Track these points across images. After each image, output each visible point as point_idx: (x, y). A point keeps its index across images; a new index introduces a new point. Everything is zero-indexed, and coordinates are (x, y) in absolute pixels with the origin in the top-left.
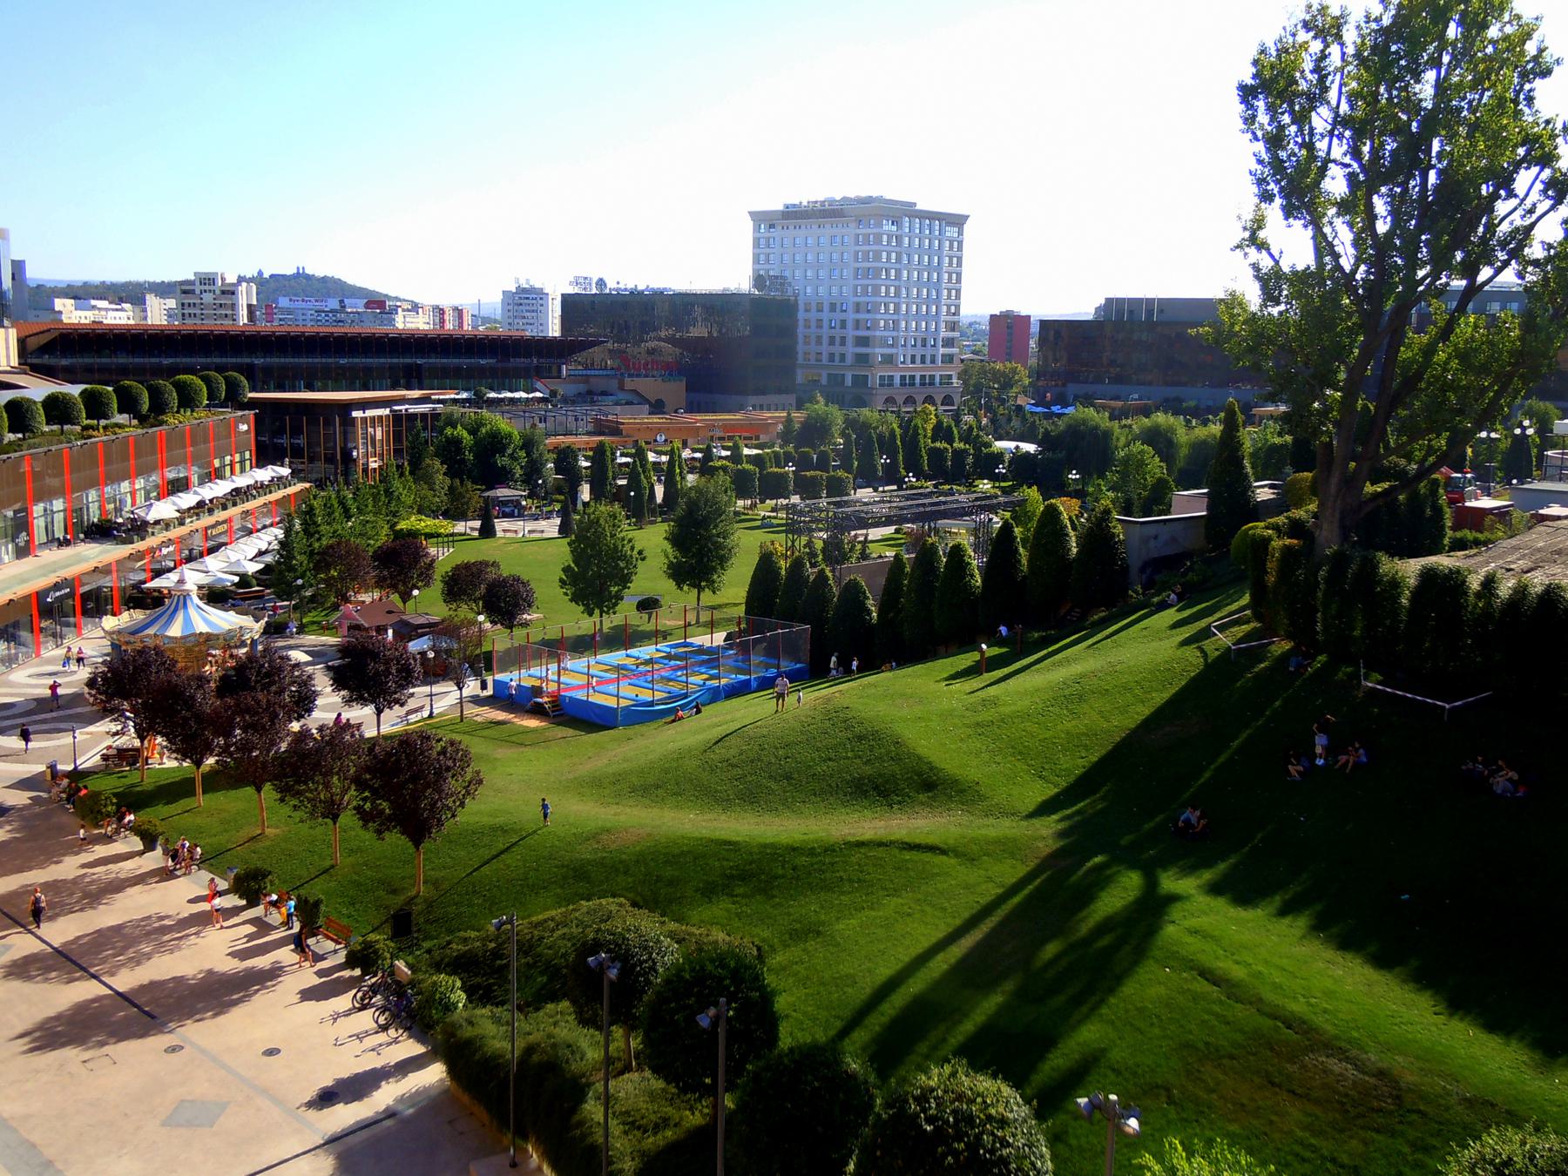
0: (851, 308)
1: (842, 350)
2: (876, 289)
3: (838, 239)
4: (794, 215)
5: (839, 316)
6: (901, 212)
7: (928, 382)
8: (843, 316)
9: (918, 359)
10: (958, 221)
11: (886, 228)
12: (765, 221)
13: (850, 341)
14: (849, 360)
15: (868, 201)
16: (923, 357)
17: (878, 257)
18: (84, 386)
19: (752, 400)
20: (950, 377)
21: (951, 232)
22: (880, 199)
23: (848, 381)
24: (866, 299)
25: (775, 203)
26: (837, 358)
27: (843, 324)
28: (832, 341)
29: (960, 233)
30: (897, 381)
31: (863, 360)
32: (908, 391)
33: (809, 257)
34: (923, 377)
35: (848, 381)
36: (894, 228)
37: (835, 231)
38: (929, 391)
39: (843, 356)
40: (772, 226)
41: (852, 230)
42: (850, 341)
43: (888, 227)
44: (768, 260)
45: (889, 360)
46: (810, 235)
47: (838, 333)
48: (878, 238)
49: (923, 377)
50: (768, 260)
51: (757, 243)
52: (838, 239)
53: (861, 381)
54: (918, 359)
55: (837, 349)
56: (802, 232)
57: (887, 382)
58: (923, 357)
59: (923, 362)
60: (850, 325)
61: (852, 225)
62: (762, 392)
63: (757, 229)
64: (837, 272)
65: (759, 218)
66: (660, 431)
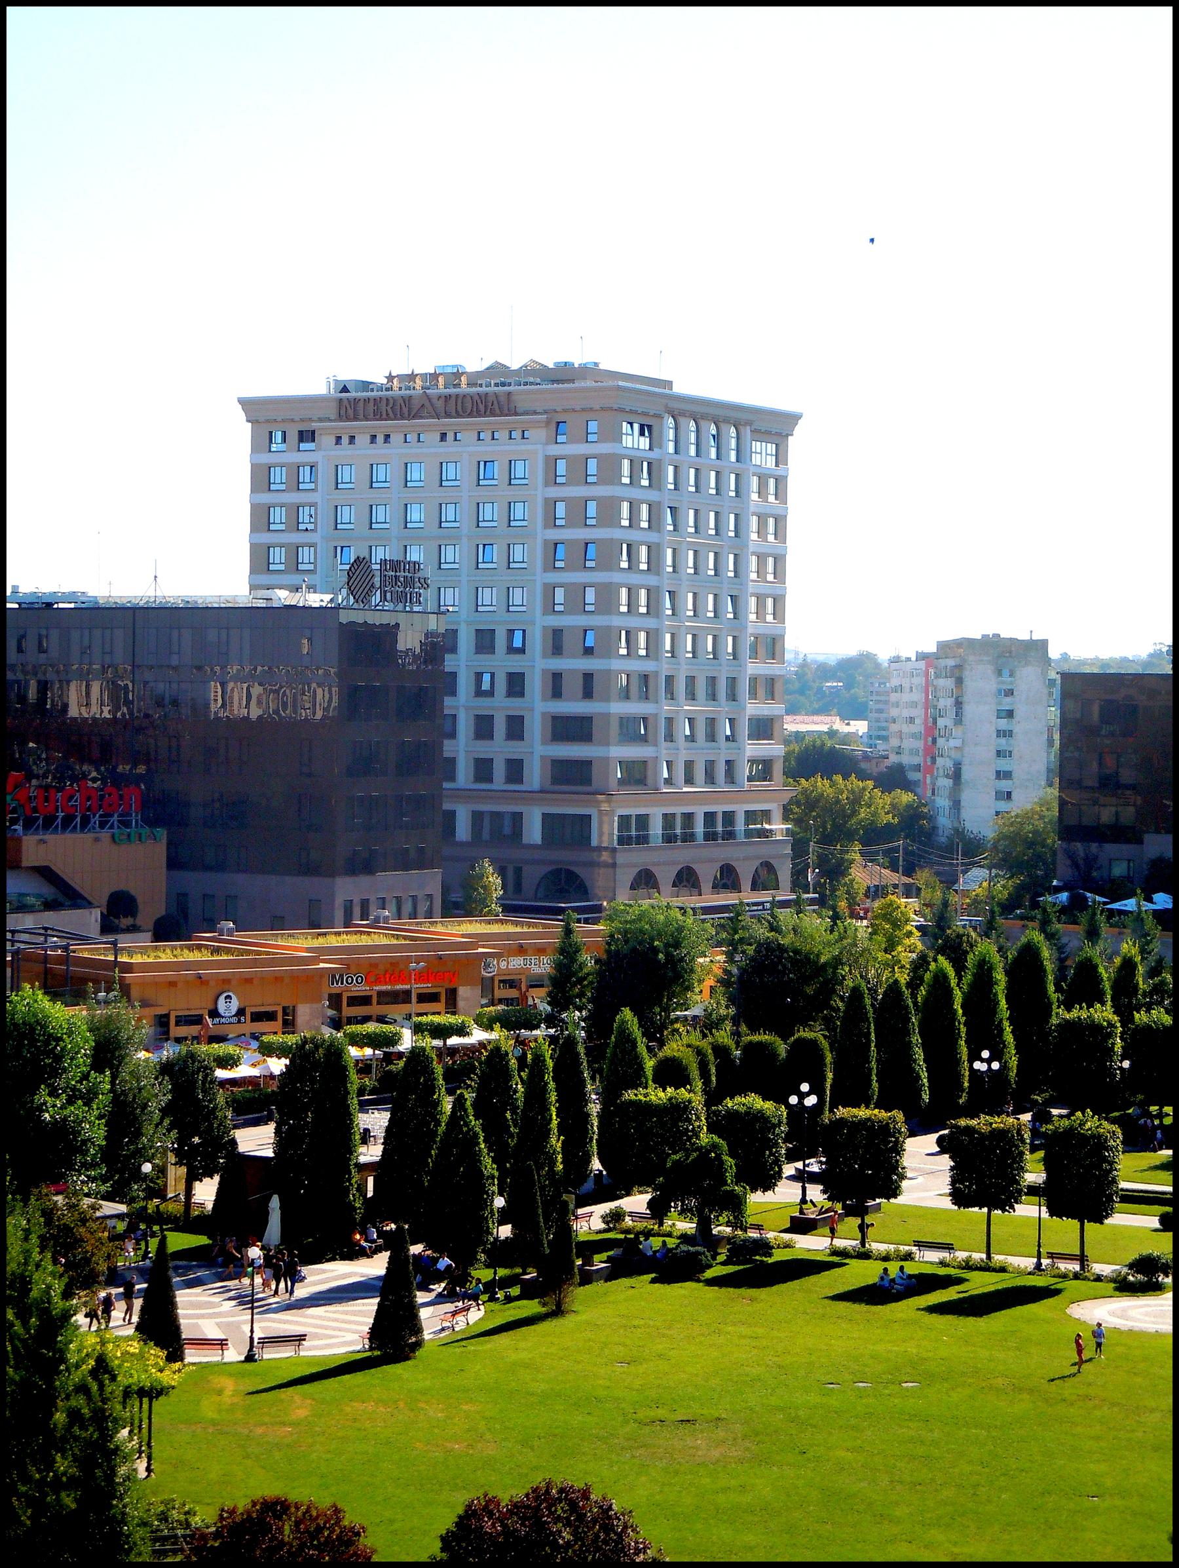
0: (537, 642)
1: (514, 749)
2: (606, 601)
3: (498, 470)
4: (366, 409)
5: (501, 663)
6: (651, 406)
7: (720, 829)
8: (515, 664)
9: (699, 773)
10: (775, 427)
11: (628, 441)
12: (279, 424)
13: (535, 728)
14: (535, 776)
15: (564, 374)
16: (710, 766)
17: (609, 514)
18: (770, 1260)
19: (346, 889)
20: (766, 815)
21: (762, 455)
22: (588, 371)
23: (534, 832)
24: (581, 621)
25: (309, 379)
26: (499, 771)
27: (516, 684)
28: (484, 727)
29: (780, 457)
30: (656, 829)
31: (573, 775)
32: (682, 855)
33: (415, 514)
34: (710, 817)
35: (534, 832)
36: (644, 443)
37: (486, 449)
38: (723, 853)
39: (515, 770)
40: (307, 436)
41: (535, 447)
42: (535, 728)
43: (633, 440)
44: (294, 524)
45: (637, 775)
46: (415, 455)
47: (501, 706)
48: (609, 466)
49: (710, 817)
50: (294, 524)
51: (261, 478)
52: (498, 470)
53: (570, 831)
54: (699, 773)
55: (499, 749)
56: (396, 450)
57: (634, 832)
58: (710, 766)
59: (710, 778)
60: (535, 685)
61: (538, 434)
62: (363, 865)
63: (262, 440)
64: (496, 553)
65: (279, 424)
66: (225, 984)
